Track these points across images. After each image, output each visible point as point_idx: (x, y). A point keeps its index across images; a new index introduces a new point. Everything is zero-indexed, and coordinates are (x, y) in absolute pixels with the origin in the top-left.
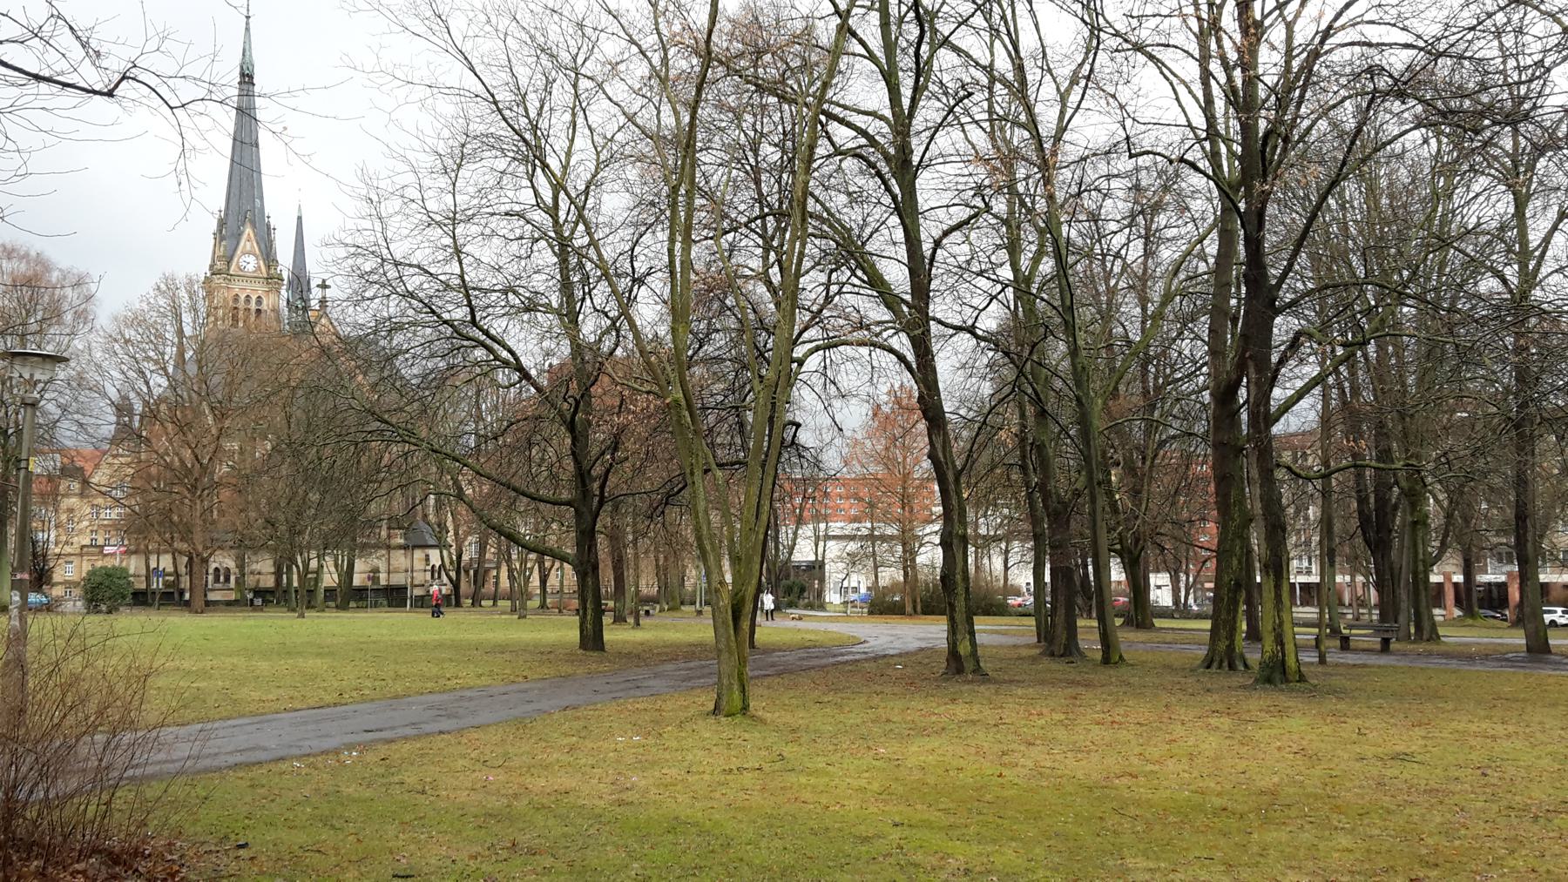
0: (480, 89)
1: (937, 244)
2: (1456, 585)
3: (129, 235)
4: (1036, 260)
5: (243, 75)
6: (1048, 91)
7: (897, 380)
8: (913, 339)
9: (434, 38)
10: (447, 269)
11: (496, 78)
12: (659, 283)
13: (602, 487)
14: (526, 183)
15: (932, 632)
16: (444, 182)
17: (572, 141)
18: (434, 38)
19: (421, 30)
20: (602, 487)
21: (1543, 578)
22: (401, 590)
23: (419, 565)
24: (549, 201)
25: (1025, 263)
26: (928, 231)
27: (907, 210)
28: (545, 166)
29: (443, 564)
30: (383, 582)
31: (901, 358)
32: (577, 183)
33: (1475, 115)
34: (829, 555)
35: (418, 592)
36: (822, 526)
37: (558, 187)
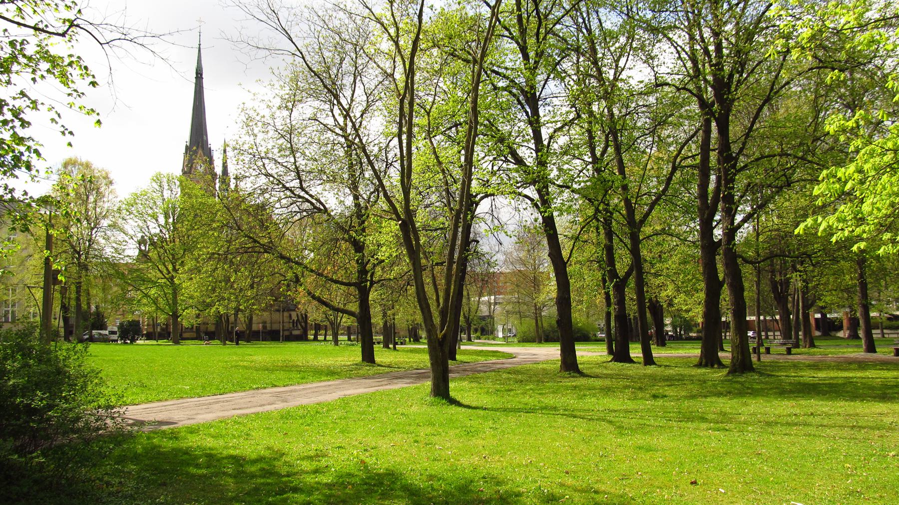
0: (293, 49)
1: (551, 137)
2: (816, 320)
3: (117, 144)
4: (604, 151)
5: (197, 73)
6: (608, 60)
7: (531, 216)
8: (539, 191)
9: (269, 22)
10: (288, 159)
11: (313, 60)
12: (397, 165)
13: (372, 276)
14: (330, 114)
15: (552, 352)
16: (286, 113)
17: (354, 91)
18: (269, 22)
19: (264, 18)
20: (372, 276)
21: (748, 319)
22: (278, 332)
23: (286, 320)
24: (342, 124)
25: (598, 151)
26: (545, 133)
27: (535, 122)
28: (339, 103)
29: (298, 319)
30: (269, 328)
31: (532, 200)
32: (356, 112)
33: (841, 65)
34: (496, 312)
35: (287, 333)
36: (493, 297)
37: (347, 115)
